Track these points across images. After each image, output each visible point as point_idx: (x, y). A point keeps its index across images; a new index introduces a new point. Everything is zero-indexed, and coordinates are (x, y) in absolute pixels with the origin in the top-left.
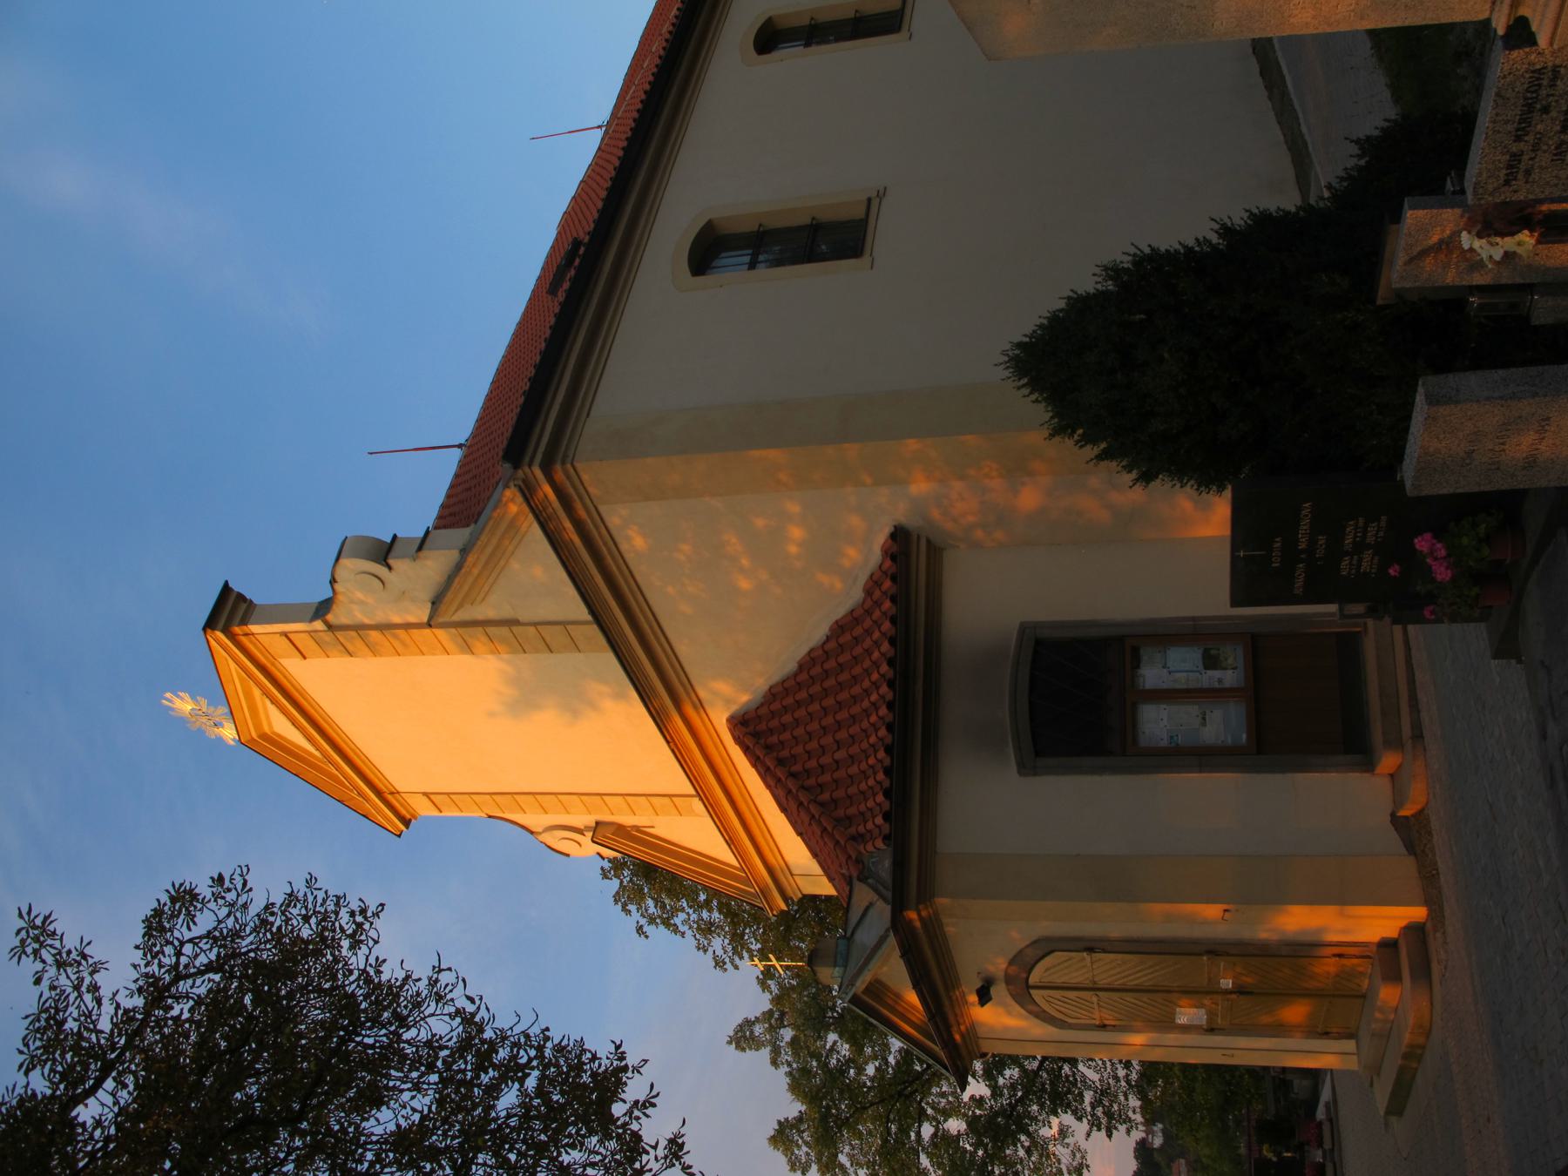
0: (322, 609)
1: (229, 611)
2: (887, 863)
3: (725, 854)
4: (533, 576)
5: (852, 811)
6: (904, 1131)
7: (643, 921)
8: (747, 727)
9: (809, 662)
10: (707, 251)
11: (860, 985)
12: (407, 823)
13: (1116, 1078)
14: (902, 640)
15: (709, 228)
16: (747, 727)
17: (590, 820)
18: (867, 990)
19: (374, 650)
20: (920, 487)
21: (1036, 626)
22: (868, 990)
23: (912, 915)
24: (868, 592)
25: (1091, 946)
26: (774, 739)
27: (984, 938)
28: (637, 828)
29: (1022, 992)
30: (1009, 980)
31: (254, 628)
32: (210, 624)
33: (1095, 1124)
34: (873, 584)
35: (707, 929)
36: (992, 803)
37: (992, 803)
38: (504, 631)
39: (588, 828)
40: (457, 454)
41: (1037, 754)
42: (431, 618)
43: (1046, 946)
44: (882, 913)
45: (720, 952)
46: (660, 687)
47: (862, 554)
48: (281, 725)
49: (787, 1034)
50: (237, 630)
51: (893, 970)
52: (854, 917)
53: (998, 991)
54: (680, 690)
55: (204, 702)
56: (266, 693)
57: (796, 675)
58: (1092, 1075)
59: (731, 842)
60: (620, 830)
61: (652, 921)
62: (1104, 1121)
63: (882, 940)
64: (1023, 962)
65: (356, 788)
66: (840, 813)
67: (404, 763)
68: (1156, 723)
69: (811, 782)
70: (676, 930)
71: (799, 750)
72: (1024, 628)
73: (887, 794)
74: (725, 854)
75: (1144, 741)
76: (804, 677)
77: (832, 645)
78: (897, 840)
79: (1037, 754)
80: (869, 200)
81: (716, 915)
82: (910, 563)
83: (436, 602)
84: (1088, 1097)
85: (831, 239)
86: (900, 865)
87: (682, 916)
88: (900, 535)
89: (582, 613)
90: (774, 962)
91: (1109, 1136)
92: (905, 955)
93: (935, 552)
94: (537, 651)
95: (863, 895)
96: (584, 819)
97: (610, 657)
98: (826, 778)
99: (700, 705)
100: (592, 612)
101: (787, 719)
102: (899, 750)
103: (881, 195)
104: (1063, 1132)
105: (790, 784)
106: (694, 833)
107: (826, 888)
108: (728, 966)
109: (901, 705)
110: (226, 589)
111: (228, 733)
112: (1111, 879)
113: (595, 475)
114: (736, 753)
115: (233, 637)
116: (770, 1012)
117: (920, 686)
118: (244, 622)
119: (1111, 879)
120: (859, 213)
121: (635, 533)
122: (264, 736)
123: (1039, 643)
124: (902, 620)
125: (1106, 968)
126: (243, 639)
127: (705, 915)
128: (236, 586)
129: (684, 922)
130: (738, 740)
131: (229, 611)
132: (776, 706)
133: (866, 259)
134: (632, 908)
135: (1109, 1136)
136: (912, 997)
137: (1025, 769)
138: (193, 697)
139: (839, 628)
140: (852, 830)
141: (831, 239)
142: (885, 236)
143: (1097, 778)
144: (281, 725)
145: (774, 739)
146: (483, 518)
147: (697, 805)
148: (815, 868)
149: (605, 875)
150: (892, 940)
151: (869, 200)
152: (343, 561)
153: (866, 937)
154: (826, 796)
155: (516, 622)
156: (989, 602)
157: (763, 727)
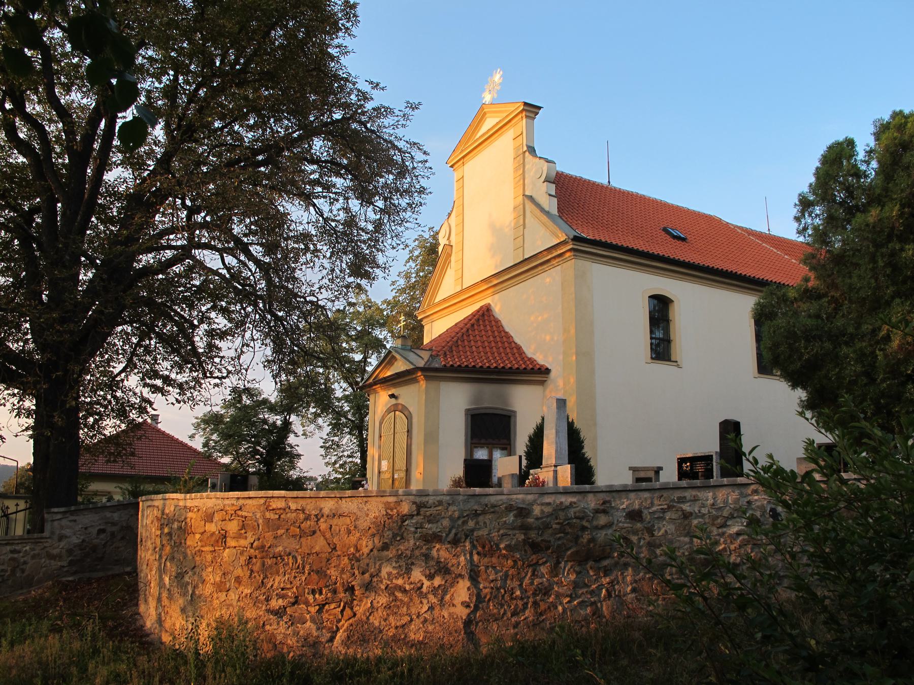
0: (532, 150)
1: (531, 110)
2: (437, 366)
3: (438, 299)
5: (455, 353)
6: (319, 359)
7: (411, 248)
8: (485, 313)
9: (508, 336)
11: (394, 353)
12: (452, 166)
13: (343, 451)
14: (518, 371)
16: (485, 313)
19: (516, 170)
20: (560, 383)
21: (515, 417)
22: (393, 357)
23: (419, 374)
24: (530, 359)
26: (481, 322)
27: (412, 396)
28: (450, 262)
29: (394, 409)
30: (396, 405)
31: (524, 120)
32: (526, 104)
33: (326, 441)
35: (407, 276)
36: (456, 400)
37: (456, 400)
38: (521, 222)
40: (605, 182)
41: (473, 416)
43: (409, 418)
44: (421, 364)
45: (398, 283)
46: (503, 278)
47: (541, 360)
48: (489, 123)
49: (361, 309)
50: (524, 114)
51: (400, 366)
52: (418, 351)
53: (393, 401)
54: (498, 288)
55: (498, 88)
56: (500, 122)
57: (504, 331)
58: (344, 441)
61: (411, 252)
62: (327, 445)
63: (412, 363)
64: (404, 410)
65: (466, 149)
66: (454, 348)
67: (474, 167)
69: (465, 337)
70: (408, 262)
71: (477, 332)
72: (515, 412)
73: (459, 366)
74: (438, 299)
75: (475, 450)
76: (503, 334)
77: (513, 345)
78: (445, 369)
79: (473, 416)
81: (414, 280)
82: (537, 374)
83: (531, 198)
84: (336, 439)
85: (662, 350)
86: (436, 370)
87: (413, 265)
88: (548, 371)
89: (526, 257)
91: (321, 447)
93: (542, 383)
95: (426, 355)
98: (466, 343)
99: (494, 294)
100: (526, 260)
102: (473, 370)
103: (678, 366)
104: (320, 428)
105: (465, 330)
107: (426, 341)
108: (393, 287)
109: (489, 371)
110: (540, 108)
111: (487, 98)
112: (431, 437)
113: (570, 267)
114: (476, 307)
115: (521, 112)
116: (371, 302)
117: (495, 377)
118: (526, 117)
119: (431, 437)
120: (673, 359)
121: (551, 280)
122: (485, 114)
123: (509, 417)
124: (525, 371)
126: (520, 116)
127: (414, 275)
128: (541, 111)
129: (411, 266)
130: (482, 307)
131: (531, 110)
132: (493, 323)
133: (757, 375)
134: (417, 243)
135: (321, 447)
136: (389, 374)
137: (467, 411)
138: (500, 84)
139: (519, 348)
141: (662, 350)
142: (661, 368)
144: (489, 123)
145: (481, 322)
146: (560, 220)
147: (459, 289)
148: (435, 335)
149: (431, 229)
150: (412, 367)
152: (546, 164)
153: (412, 356)
154: (460, 343)
155: (524, 228)
157: (486, 318)
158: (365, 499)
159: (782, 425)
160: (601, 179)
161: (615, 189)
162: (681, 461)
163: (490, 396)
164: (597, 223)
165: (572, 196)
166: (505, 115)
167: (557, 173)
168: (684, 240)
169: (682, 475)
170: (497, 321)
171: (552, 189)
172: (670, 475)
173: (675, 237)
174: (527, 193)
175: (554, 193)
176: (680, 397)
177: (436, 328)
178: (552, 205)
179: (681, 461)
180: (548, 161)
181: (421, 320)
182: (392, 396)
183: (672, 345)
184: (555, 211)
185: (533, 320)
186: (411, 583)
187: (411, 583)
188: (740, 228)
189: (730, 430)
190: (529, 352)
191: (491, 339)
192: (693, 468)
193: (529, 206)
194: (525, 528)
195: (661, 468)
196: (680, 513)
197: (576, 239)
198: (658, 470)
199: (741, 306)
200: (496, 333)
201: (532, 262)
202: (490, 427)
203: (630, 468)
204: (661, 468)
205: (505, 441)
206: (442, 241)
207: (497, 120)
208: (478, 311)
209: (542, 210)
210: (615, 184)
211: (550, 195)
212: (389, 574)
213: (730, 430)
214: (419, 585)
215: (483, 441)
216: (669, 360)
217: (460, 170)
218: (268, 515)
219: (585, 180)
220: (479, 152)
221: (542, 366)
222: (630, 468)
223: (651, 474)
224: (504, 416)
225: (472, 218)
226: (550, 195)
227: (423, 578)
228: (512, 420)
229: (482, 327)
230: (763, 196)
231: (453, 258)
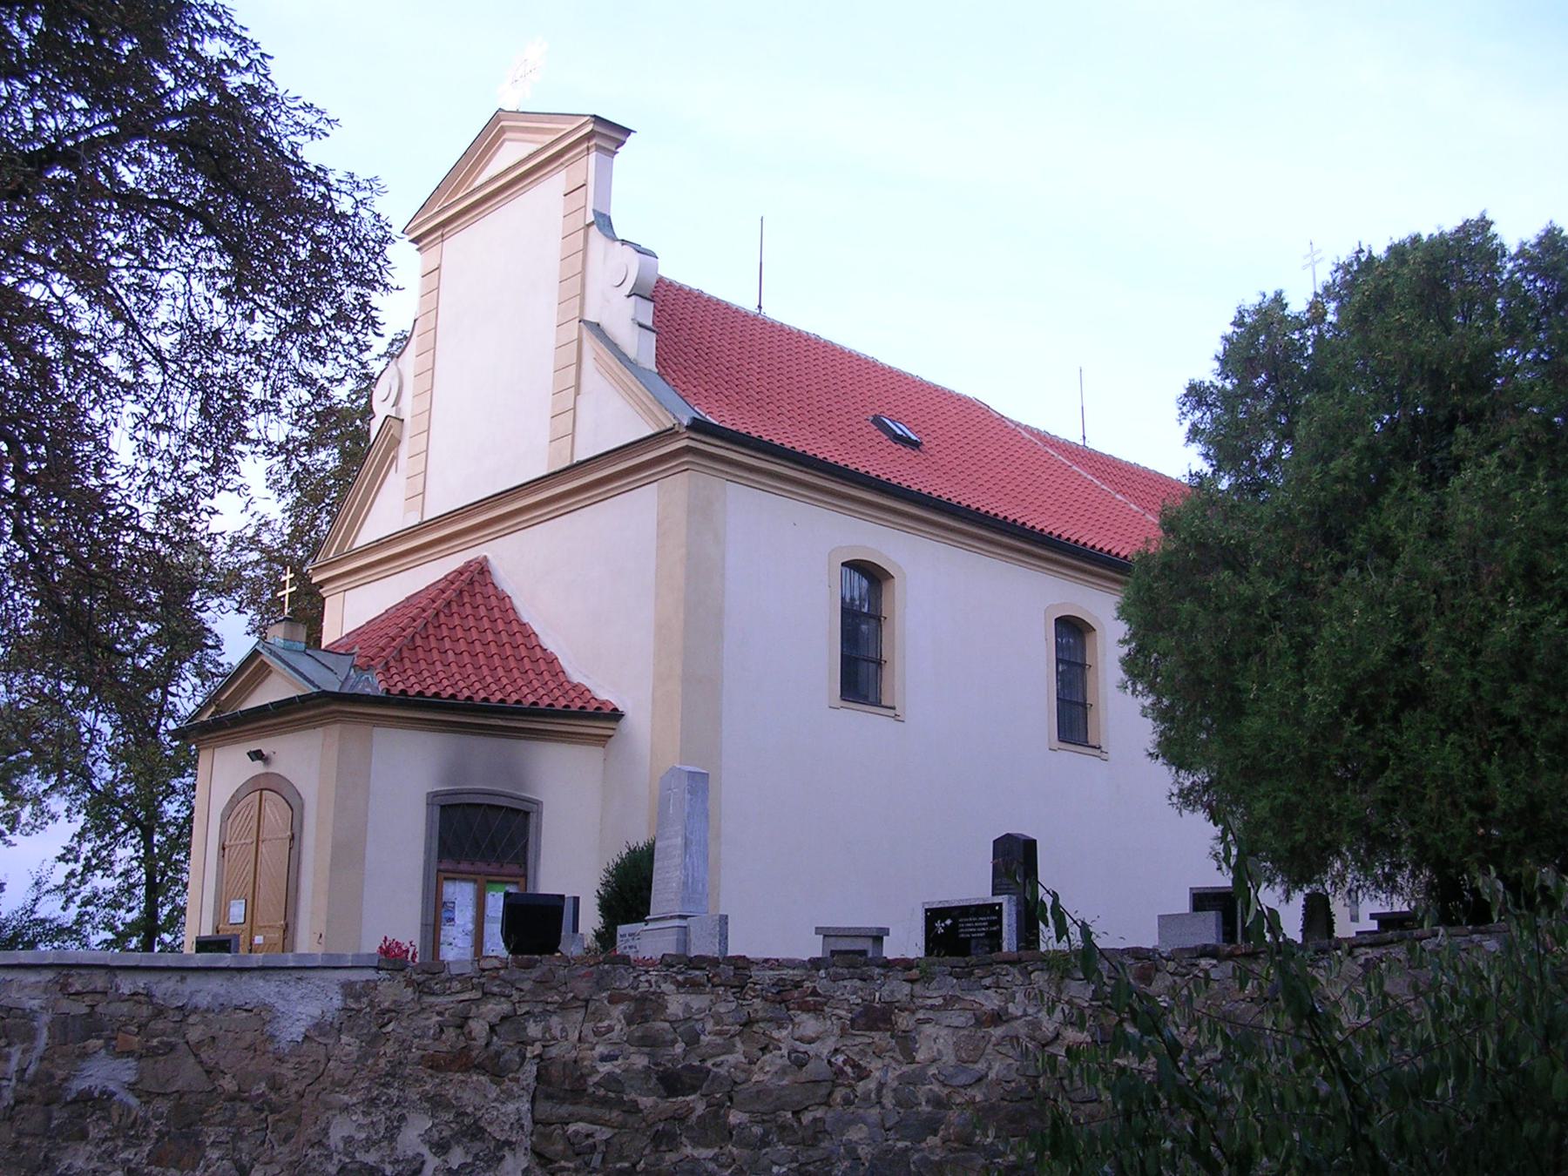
0: (603, 222)
3: (366, 536)
4: (615, 418)
5: (407, 664)
9: (527, 633)
10: (871, 575)
14: (551, 713)
15: (888, 576)
17: (406, 415)
18: (263, 663)
21: (539, 814)
24: (575, 687)
25: (294, 839)
27: (301, 757)
28: (394, 458)
32: (597, 119)
34: (581, 691)
36: (408, 772)
37: (408, 772)
39: (398, 411)
40: (751, 307)
41: (442, 807)
42: (585, 322)
48: (510, 154)
53: (258, 767)
59: (380, 544)
60: (396, 442)
66: (406, 653)
68: (461, 894)
69: (431, 631)
72: (538, 803)
79: (442, 807)
80: (893, 708)
82: (592, 720)
83: (596, 328)
85: (861, 673)
88: (616, 715)
89: (581, 456)
90: (288, 590)
92: (290, 701)
93: (602, 740)
94: (554, 405)
96: (407, 409)
97: (545, 473)
101: (482, 611)
106: (387, 512)
109: (469, 707)
110: (628, 132)
117: (501, 723)
120: (1092, 741)
121: (637, 513)
122: (503, 130)
123: (527, 814)
125: (273, 855)
128: (630, 140)
133: (837, 701)
137: (433, 797)
139: (552, 661)
140: (392, 663)
141: (861, 673)
142: (859, 719)
143: (422, 849)
144: (510, 154)
151: (893, 708)
154: (419, 641)
155: (577, 393)
156: (560, 780)
158: (297, 974)
159: (1138, 850)
160: (744, 300)
161: (773, 325)
162: (933, 915)
163: (481, 764)
164: (737, 400)
165: (688, 330)
166: (549, 139)
167: (661, 280)
168: (915, 445)
169: (934, 942)
170: (503, 598)
171: (647, 313)
172: (906, 942)
173: (897, 438)
174: (589, 317)
175: (649, 323)
176: (919, 784)
177: (351, 610)
178: (643, 348)
179: (933, 915)
180: (639, 250)
181: (321, 584)
182: (257, 755)
183: (886, 670)
184: (649, 362)
185: (582, 594)
186: (397, 1161)
187: (397, 1161)
188: (1026, 428)
189: (1016, 858)
190: (576, 673)
191: (490, 636)
192: (954, 934)
193: (590, 345)
194: (649, 1042)
195: (886, 931)
196: (969, 1014)
197: (698, 426)
198: (878, 937)
199: (1037, 596)
200: (500, 626)
201: (592, 472)
202: (484, 834)
203: (818, 930)
204: (886, 931)
205: (514, 868)
206: (381, 410)
207: (533, 148)
208: (460, 572)
209: (622, 357)
210: (780, 311)
211: (641, 325)
212: (348, 1140)
213: (1016, 858)
214: (416, 1165)
215: (464, 866)
216: (878, 703)
217: (435, 251)
218: (67, 1006)
219: (710, 299)
220: (484, 215)
221: (604, 703)
222: (818, 930)
223: (866, 945)
224: (518, 811)
225: (479, 373)
226: (641, 325)
227: (425, 1150)
228: (533, 819)
229: (468, 609)
230: (1119, 385)
231: (404, 451)
